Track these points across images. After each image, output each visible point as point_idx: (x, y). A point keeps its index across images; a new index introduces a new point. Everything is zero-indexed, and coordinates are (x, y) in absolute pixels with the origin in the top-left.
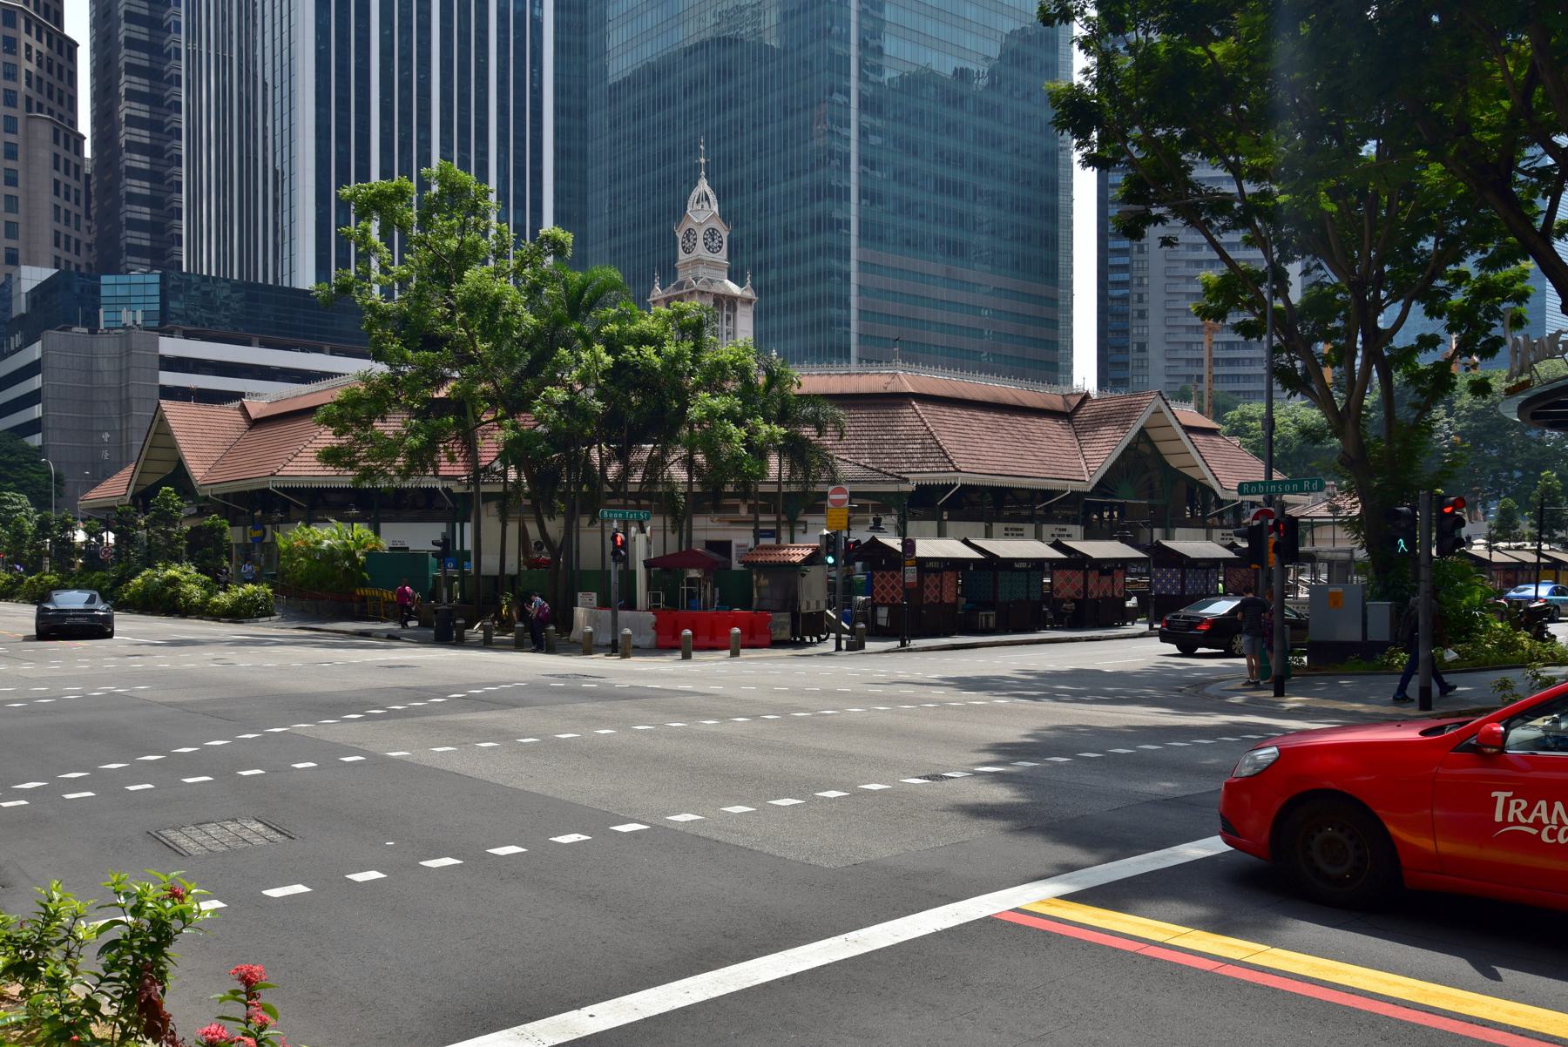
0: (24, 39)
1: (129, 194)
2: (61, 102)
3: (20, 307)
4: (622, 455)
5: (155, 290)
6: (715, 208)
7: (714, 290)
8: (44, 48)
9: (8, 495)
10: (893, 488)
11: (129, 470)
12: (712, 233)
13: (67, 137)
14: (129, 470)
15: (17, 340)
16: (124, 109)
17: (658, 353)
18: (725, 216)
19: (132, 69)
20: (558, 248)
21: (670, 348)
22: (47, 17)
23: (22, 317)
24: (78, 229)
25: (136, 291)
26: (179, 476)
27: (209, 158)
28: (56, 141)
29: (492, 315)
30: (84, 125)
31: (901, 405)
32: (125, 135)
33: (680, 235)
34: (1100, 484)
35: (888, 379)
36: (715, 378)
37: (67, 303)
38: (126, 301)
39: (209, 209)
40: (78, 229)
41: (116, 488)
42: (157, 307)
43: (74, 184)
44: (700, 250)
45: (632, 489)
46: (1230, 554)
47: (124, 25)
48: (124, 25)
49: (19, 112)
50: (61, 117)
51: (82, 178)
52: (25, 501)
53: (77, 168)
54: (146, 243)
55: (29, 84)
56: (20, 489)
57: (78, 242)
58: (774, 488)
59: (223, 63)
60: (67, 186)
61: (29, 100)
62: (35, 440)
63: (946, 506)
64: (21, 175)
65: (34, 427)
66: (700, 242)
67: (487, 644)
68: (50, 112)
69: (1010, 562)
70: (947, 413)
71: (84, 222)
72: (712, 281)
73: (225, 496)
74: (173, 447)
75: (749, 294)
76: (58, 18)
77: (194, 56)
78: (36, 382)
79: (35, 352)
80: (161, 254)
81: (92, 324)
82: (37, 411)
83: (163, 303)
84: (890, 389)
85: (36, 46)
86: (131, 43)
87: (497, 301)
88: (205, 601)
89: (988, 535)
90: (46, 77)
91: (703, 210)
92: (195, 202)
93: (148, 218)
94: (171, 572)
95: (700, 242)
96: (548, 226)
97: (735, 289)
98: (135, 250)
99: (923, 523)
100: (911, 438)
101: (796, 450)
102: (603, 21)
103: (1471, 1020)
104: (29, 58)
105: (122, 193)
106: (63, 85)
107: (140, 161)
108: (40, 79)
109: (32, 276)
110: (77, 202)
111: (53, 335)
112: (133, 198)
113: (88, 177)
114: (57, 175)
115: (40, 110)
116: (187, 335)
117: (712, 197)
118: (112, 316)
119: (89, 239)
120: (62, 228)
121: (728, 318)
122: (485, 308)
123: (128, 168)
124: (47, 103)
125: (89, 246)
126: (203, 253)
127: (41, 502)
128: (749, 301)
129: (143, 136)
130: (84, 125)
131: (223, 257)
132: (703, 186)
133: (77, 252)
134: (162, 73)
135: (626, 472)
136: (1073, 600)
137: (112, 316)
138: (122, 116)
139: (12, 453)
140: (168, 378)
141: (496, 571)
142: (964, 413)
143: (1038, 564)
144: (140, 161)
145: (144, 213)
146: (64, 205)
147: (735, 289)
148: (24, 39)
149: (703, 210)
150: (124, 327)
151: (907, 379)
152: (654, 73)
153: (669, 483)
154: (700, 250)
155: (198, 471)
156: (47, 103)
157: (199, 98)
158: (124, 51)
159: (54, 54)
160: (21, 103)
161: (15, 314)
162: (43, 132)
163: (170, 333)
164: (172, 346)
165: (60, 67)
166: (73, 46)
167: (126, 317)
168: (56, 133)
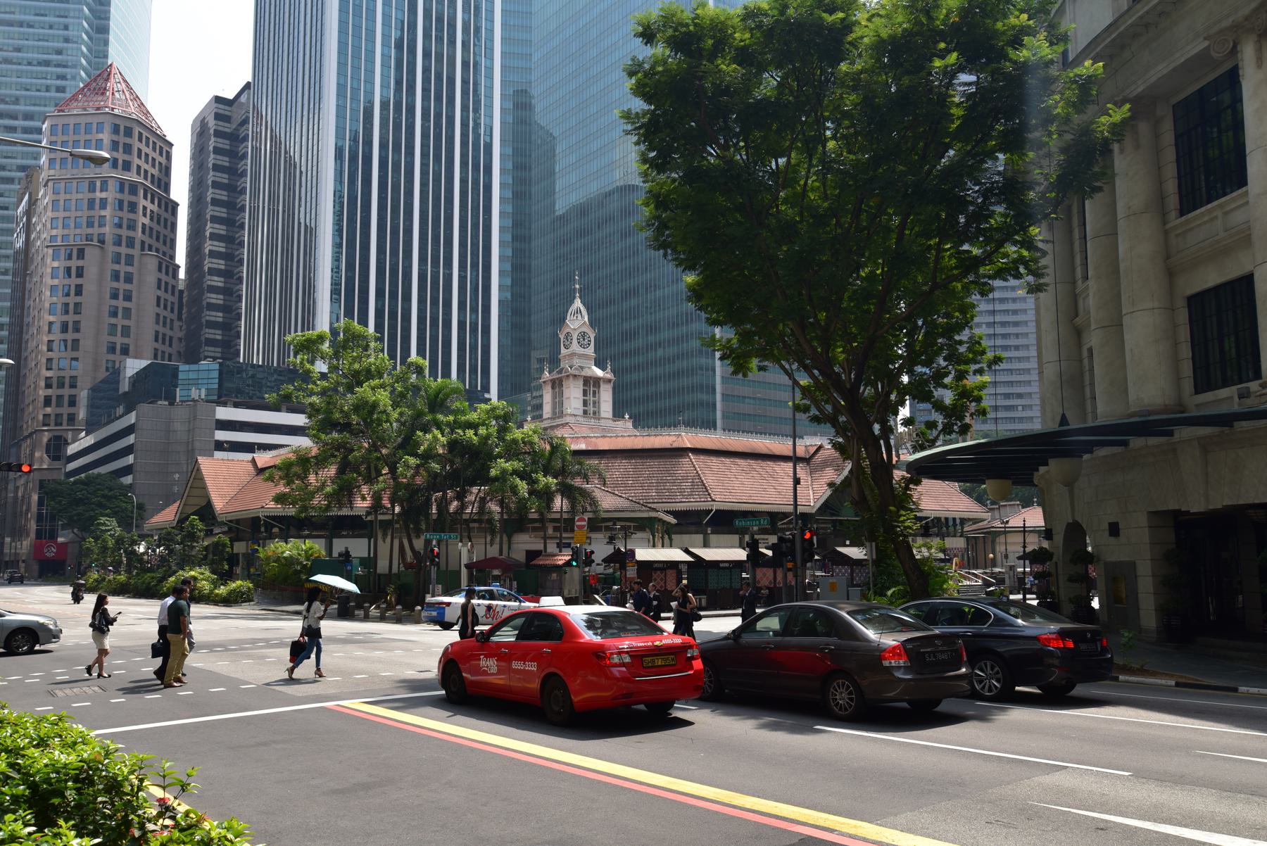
0: (143, 202)
1: (208, 304)
2: (165, 243)
3: (125, 387)
4: (460, 497)
5: (216, 374)
6: (586, 319)
7: (583, 373)
8: (155, 208)
9: (103, 520)
10: (645, 515)
11: (177, 504)
12: (583, 335)
13: (167, 267)
14: (177, 504)
15: (121, 410)
16: (208, 246)
17: (476, 434)
18: (592, 323)
19: (215, 219)
20: (419, 370)
21: (482, 431)
22: (159, 187)
23: (126, 393)
24: (171, 329)
25: (202, 375)
26: (206, 512)
27: (261, 280)
28: (160, 270)
29: (371, 413)
30: (181, 258)
31: (681, 456)
32: (208, 264)
33: (562, 337)
34: (820, 509)
35: (674, 438)
36: (512, 451)
37: (156, 384)
38: (196, 383)
39: (259, 314)
40: (171, 329)
41: (167, 516)
42: (216, 386)
43: (170, 298)
44: (575, 347)
45: (465, 517)
46: (689, 558)
47: (211, 190)
48: (211, 190)
49: (136, 252)
50: (164, 254)
51: (177, 294)
52: (115, 523)
53: (173, 287)
54: (219, 337)
55: (143, 232)
56: (114, 514)
57: (171, 338)
58: (558, 516)
59: (273, 213)
60: (166, 300)
61: (143, 243)
62: (128, 480)
63: (708, 524)
64: (134, 294)
65: (128, 470)
66: (575, 341)
67: (382, 619)
68: (157, 250)
69: (715, 564)
70: (714, 461)
71: (177, 324)
72: (582, 368)
73: (238, 521)
74: (204, 488)
75: (609, 376)
76: (167, 188)
77: (254, 211)
78: (131, 439)
79: (132, 418)
80: (228, 346)
81: (171, 399)
82: (130, 459)
83: (220, 384)
84: (675, 445)
85: (150, 206)
86: (215, 202)
87: (375, 405)
88: (211, 591)
89: (706, 545)
90: (156, 227)
91: (578, 319)
92: (251, 309)
93: (221, 320)
94: (193, 573)
95: (575, 341)
96: (413, 356)
97: (599, 372)
98: (211, 342)
99: (694, 536)
100: (685, 479)
101: (567, 491)
102: (552, 173)
103: (735, 807)
104: (145, 215)
105: (204, 303)
106: (167, 232)
107: (218, 281)
108: (151, 229)
109: (133, 366)
110: (172, 311)
111: (144, 407)
112: (211, 307)
113: (181, 292)
114: (159, 293)
115: (150, 249)
116: (236, 405)
117: (583, 309)
118: (185, 393)
119: (181, 334)
120: (161, 329)
121: (594, 393)
122: (367, 409)
123: (209, 286)
124: (155, 244)
125: (180, 339)
126: (254, 349)
127: (126, 523)
128: (610, 381)
129: (220, 264)
130: (181, 258)
131: (267, 350)
132: (578, 303)
133: (170, 345)
134: (235, 222)
135: (463, 506)
136: (767, 588)
137: (185, 393)
138: (207, 251)
139: (111, 489)
140: (221, 435)
141: (387, 571)
142: (727, 461)
143: (737, 564)
144: (218, 281)
145: (218, 317)
146: (163, 313)
147: (599, 372)
148: (143, 202)
149: (578, 319)
150: (193, 400)
151: (687, 438)
152: (582, 210)
153: (490, 512)
154: (575, 347)
155: (219, 504)
156: (155, 244)
157: (258, 237)
158: (210, 207)
159: (162, 212)
160: (138, 245)
161: (121, 392)
162: (152, 264)
163: (224, 404)
164: (224, 413)
165: (166, 220)
166: (175, 205)
167: (194, 393)
168: (160, 264)
